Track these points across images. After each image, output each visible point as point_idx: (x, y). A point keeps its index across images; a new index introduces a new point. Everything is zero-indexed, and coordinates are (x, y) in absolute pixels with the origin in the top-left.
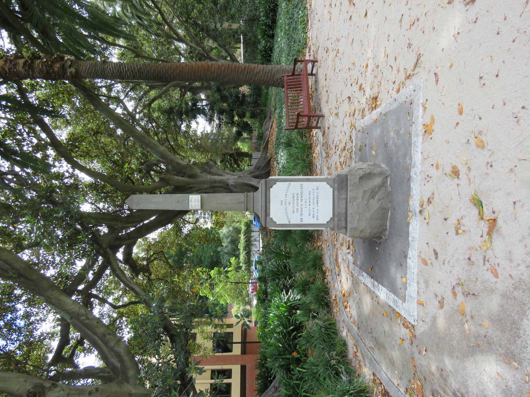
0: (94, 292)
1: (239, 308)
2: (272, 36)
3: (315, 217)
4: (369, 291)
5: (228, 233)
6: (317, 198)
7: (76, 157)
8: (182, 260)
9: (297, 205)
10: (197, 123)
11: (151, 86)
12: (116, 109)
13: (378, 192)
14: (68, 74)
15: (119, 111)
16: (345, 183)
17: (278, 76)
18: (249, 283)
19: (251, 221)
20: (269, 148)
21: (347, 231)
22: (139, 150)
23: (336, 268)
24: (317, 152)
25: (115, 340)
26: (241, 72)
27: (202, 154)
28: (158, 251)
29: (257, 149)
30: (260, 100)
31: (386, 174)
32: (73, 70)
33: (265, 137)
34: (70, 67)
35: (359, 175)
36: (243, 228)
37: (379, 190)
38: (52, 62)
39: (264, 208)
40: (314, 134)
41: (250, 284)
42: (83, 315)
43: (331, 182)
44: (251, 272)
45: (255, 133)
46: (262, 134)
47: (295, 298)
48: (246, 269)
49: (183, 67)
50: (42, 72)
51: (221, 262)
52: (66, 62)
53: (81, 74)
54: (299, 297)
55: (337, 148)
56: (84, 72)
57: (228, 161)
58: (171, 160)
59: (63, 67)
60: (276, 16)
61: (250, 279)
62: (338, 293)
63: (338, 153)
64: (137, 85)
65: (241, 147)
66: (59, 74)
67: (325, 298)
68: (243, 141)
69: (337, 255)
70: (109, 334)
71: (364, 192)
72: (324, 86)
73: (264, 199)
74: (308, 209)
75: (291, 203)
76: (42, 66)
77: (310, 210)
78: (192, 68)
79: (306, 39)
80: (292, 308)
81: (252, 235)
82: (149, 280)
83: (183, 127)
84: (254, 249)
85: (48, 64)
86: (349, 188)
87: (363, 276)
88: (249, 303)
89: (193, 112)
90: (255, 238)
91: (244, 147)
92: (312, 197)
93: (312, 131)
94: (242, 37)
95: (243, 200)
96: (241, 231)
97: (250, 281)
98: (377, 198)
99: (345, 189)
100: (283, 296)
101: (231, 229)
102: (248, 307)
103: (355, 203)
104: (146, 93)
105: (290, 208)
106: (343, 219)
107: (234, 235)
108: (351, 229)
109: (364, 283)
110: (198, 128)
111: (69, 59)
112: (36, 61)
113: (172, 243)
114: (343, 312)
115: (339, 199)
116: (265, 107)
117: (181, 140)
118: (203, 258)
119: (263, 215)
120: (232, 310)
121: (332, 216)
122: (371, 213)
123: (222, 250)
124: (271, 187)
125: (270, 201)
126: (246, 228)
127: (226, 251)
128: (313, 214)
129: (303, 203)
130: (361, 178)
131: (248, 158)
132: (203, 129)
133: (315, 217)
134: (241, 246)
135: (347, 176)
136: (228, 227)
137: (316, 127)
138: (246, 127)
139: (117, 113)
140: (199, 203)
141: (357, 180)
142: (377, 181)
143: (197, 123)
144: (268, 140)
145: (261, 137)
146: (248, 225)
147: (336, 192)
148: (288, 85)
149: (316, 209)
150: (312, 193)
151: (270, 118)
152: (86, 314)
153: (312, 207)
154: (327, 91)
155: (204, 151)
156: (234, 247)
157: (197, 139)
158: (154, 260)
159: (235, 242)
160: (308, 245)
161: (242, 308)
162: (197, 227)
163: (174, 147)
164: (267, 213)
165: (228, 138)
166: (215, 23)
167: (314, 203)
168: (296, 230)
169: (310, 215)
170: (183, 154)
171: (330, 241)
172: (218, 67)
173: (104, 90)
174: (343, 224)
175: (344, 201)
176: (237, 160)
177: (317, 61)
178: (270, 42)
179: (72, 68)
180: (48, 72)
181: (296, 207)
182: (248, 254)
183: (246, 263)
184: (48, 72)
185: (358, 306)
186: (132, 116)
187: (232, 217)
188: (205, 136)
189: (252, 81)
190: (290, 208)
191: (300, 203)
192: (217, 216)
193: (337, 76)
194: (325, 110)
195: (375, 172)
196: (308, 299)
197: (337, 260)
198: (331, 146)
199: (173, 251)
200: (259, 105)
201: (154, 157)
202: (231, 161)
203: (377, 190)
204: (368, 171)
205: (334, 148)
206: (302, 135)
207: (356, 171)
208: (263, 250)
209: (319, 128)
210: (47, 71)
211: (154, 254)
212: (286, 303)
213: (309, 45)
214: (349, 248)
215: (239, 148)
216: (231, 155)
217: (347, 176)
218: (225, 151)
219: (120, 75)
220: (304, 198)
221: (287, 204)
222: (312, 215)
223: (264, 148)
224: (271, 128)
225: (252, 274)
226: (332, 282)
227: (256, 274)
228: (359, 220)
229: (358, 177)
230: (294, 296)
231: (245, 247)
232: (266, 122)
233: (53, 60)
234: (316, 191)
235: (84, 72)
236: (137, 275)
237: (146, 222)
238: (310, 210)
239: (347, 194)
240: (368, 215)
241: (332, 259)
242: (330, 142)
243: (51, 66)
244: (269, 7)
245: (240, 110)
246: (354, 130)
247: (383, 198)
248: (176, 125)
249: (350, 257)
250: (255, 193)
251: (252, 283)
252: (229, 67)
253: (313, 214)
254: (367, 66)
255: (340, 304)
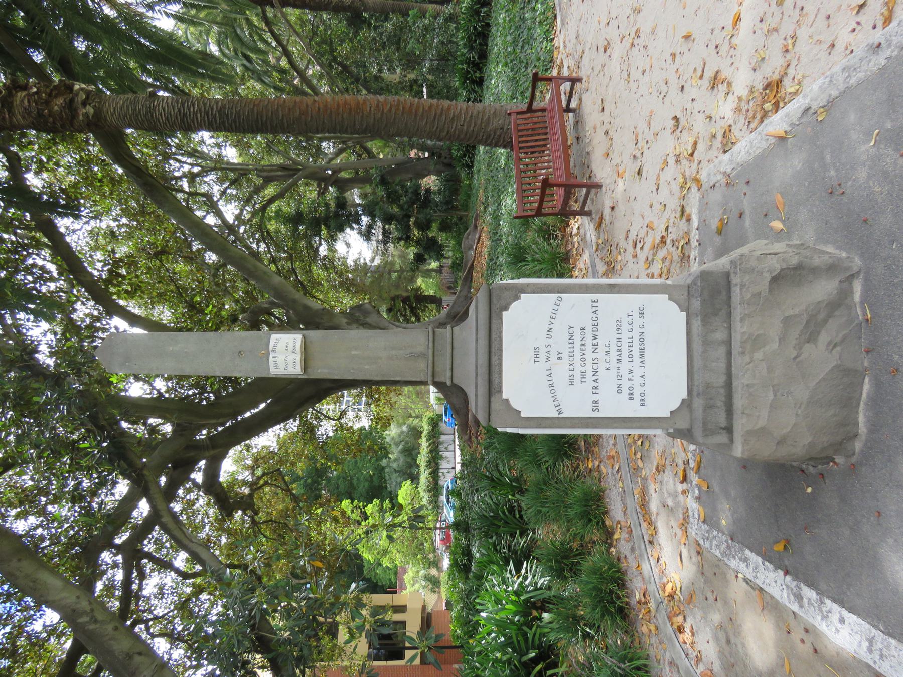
0: (149, 547)
1: (418, 572)
2: (480, 82)
3: (637, 397)
4: (769, 605)
5: (400, 436)
6: (642, 340)
7: (118, 294)
8: (319, 484)
9: (583, 360)
10: (348, 245)
11: (267, 177)
12: (204, 217)
13: (825, 321)
14: (81, 118)
15: (211, 220)
16: (724, 296)
17: (496, 123)
18: (436, 528)
19: (440, 416)
20: (474, 278)
21: (732, 440)
22: (240, 285)
23: (644, 525)
24: (582, 266)
25: (153, 667)
26: (422, 116)
27: (353, 297)
28: (272, 469)
29: (451, 288)
30: (456, 200)
31: (848, 269)
32: (90, 110)
33: (467, 262)
34: (84, 104)
35: (770, 271)
36: (426, 428)
37: (830, 316)
38: (50, 95)
39: (483, 370)
40: (575, 231)
41: (438, 531)
42: (84, 613)
43: (684, 297)
44: (439, 507)
45: (450, 255)
46: (461, 259)
47: (536, 584)
48: (430, 502)
49: (307, 106)
50: (29, 114)
51: (386, 487)
52: (77, 95)
53: (106, 120)
54: (543, 581)
55: (639, 245)
56: (112, 115)
57: (400, 311)
58: (295, 301)
59: (70, 105)
60: (487, 45)
61: (437, 520)
62: (652, 588)
63: (642, 256)
64: (242, 175)
65: (423, 286)
66: (61, 119)
67: (618, 598)
68: (427, 274)
69: (644, 493)
70: (140, 654)
71: (787, 321)
72: (598, 126)
73: (483, 342)
74: (613, 372)
75: (565, 356)
76: (29, 102)
77: (620, 377)
78: (326, 106)
79: (551, 52)
80: (532, 607)
81: (441, 440)
82: (254, 522)
83: (323, 250)
84: (444, 465)
85: (40, 98)
86: (738, 312)
87: (746, 560)
88: (436, 564)
89: (338, 219)
90: (446, 445)
91: (426, 285)
92: (625, 336)
93: (568, 225)
94: (425, 90)
95: (421, 348)
96: (421, 433)
97: (438, 525)
98: (824, 338)
99: (723, 313)
100: (508, 575)
101: (405, 428)
102: (434, 572)
103: (759, 355)
104: (258, 190)
105: (561, 371)
106: (720, 404)
107: (411, 440)
108: (750, 433)
109: (746, 580)
110: (350, 254)
111: (82, 89)
112: (19, 94)
113: (300, 455)
114: (673, 646)
115: (706, 343)
116: (466, 210)
117: (318, 272)
118: (355, 482)
119: (482, 389)
120: (405, 577)
121: (684, 395)
122: (812, 384)
123: (388, 466)
124: (506, 308)
125: (501, 350)
126: (430, 428)
127: (395, 465)
128: (631, 388)
129: (601, 353)
130: (776, 280)
131: (434, 306)
132: (357, 256)
133: (637, 397)
134: (422, 460)
135: (727, 275)
136: (400, 425)
137: (582, 213)
138: (431, 248)
139: (208, 225)
140: (298, 357)
141: (763, 285)
142: (823, 289)
143: (348, 245)
144: (472, 265)
145: (457, 266)
146: (435, 423)
147: (697, 324)
148: (519, 131)
149: (638, 371)
150: (625, 327)
151: (476, 227)
152: (92, 610)
153: (625, 366)
154: (606, 133)
155: (356, 292)
156: (409, 460)
157: (347, 272)
158: (263, 485)
159: (411, 452)
160: (565, 468)
161: (422, 573)
162: (342, 426)
163: (305, 283)
164: (493, 386)
165: (402, 271)
166: (378, 64)
167: (631, 356)
168: (536, 436)
169: (619, 391)
170: (321, 297)
171: (623, 457)
172: (378, 106)
173: (185, 184)
174: (722, 420)
175: (722, 351)
176: (416, 308)
177: (579, 80)
178: (476, 92)
179: (88, 107)
180: (40, 114)
181: (578, 368)
182: (435, 474)
183: (430, 491)
184: (40, 114)
185: (722, 635)
186: (232, 229)
187: (406, 408)
188: (361, 269)
189: (444, 134)
190: (561, 371)
191: (589, 355)
192: (378, 405)
193: (634, 89)
194: (602, 172)
195: (817, 261)
196: (571, 589)
197: (644, 505)
198: (622, 244)
199: (301, 467)
200: (455, 208)
201: (265, 299)
202: (405, 309)
203: (822, 316)
204: (795, 261)
205: (630, 249)
206: (546, 233)
207: (758, 259)
208: (462, 471)
209: (588, 214)
210: (38, 112)
211: (264, 474)
212: (516, 593)
213: (558, 62)
214: (685, 479)
215: (419, 289)
216: (406, 300)
217: (727, 275)
218: (394, 293)
219: (182, 121)
220: (601, 341)
221: (554, 357)
222: (626, 392)
223: (465, 279)
224: (478, 243)
225: (440, 510)
226: (631, 558)
227: (449, 515)
228: (773, 407)
229: (768, 277)
230: (535, 577)
231: (429, 461)
232: (469, 234)
233: (52, 90)
234: (638, 322)
235: (112, 115)
236: (230, 515)
237: (248, 414)
238: (620, 377)
239: (730, 328)
240: (801, 392)
241: (629, 502)
242: (620, 237)
243: (47, 103)
244: (475, 28)
245: (421, 216)
246: (694, 189)
247: (843, 340)
248: (310, 246)
249: (693, 505)
250: (456, 329)
251: (441, 528)
252: (398, 105)
253: (631, 388)
254: (738, 19)
255: (662, 618)
